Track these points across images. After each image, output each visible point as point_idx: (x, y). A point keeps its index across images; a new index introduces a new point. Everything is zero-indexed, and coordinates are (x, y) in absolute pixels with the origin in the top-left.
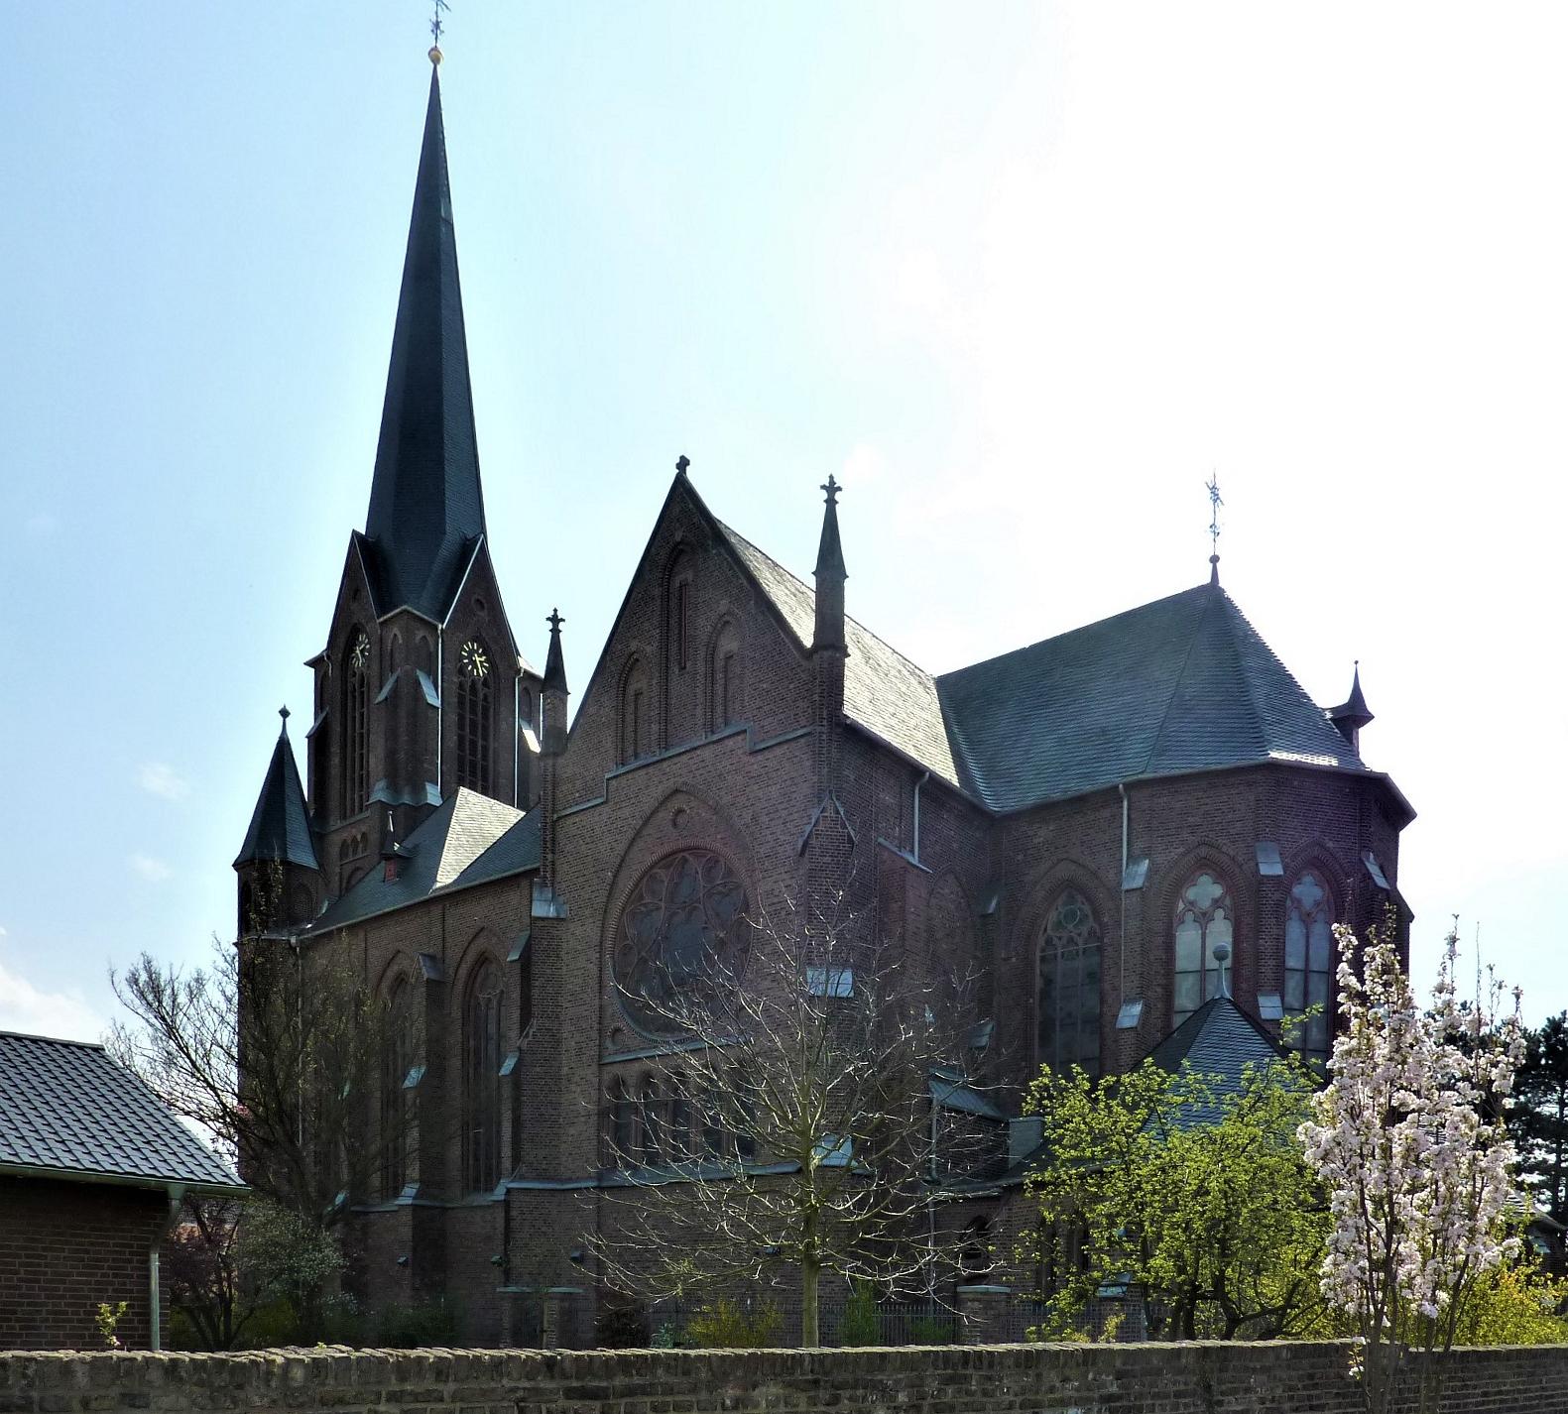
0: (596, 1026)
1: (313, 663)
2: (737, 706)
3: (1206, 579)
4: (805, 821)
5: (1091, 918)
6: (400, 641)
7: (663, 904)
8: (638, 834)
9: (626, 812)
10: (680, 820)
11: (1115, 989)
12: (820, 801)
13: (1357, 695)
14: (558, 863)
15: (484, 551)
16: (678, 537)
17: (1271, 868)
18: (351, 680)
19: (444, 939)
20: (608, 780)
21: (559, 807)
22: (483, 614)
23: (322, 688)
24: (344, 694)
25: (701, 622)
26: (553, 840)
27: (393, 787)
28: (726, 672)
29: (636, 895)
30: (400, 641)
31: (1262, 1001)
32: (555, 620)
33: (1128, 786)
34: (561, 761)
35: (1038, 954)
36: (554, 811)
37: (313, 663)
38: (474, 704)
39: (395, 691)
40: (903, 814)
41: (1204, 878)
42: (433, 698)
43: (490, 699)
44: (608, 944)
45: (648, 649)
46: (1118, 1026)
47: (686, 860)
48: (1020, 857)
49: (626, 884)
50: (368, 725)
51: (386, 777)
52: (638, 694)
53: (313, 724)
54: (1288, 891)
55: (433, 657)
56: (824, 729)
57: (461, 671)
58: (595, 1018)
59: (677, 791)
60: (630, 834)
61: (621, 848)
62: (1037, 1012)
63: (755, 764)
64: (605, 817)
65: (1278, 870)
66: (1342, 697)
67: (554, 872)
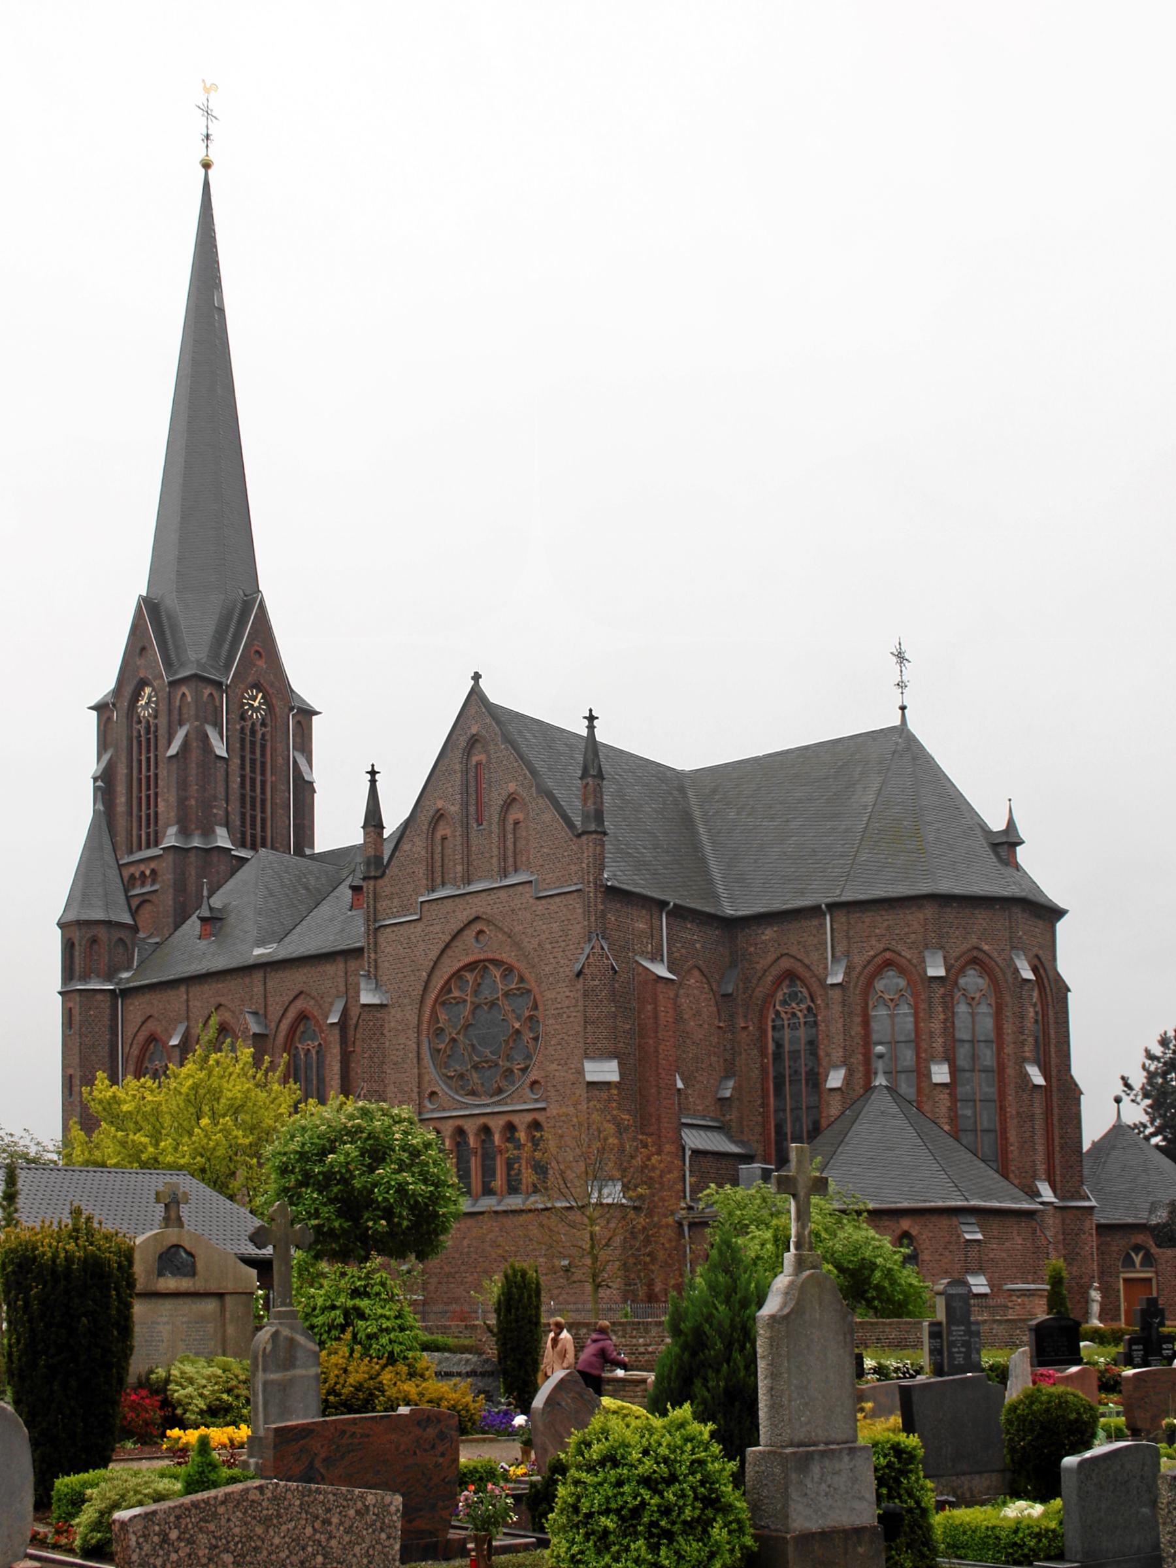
0: (416, 1090)
1: (99, 708)
2: (524, 859)
3: (898, 723)
4: (579, 951)
5: (809, 1000)
6: (189, 699)
7: (468, 998)
8: (448, 946)
9: (437, 928)
10: (481, 938)
11: (828, 1055)
12: (590, 940)
13: (1011, 823)
14: (380, 960)
15: (262, 606)
16: (474, 730)
17: (936, 970)
18: (136, 726)
19: (265, 997)
20: (422, 902)
21: (379, 917)
22: (261, 663)
23: (105, 732)
24: (130, 739)
25: (494, 795)
26: (376, 944)
27: (184, 832)
28: (514, 834)
29: (446, 988)
30: (189, 699)
31: (934, 1068)
32: (373, 773)
33: (831, 906)
34: (381, 882)
35: (770, 1024)
36: (375, 921)
37: (99, 708)
38: (253, 743)
39: (185, 745)
40: (653, 933)
41: (891, 973)
42: (221, 750)
43: (268, 737)
44: (425, 1026)
45: (452, 809)
46: (927, 953)
47: (486, 967)
48: (752, 949)
49: (438, 983)
50: (156, 768)
51: (178, 822)
52: (444, 838)
53: (95, 766)
54: (956, 983)
55: (217, 711)
56: (591, 890)
57: (243, 717)
58: (415, 1084)
59: (477, 918)
60: (442, 945)
61: (433, 955)
62: (771, 1069)
63: (540, 907)
64: (419, 929)
65: (941, 972)
66: (1003, 827)
67: (376, 967)
